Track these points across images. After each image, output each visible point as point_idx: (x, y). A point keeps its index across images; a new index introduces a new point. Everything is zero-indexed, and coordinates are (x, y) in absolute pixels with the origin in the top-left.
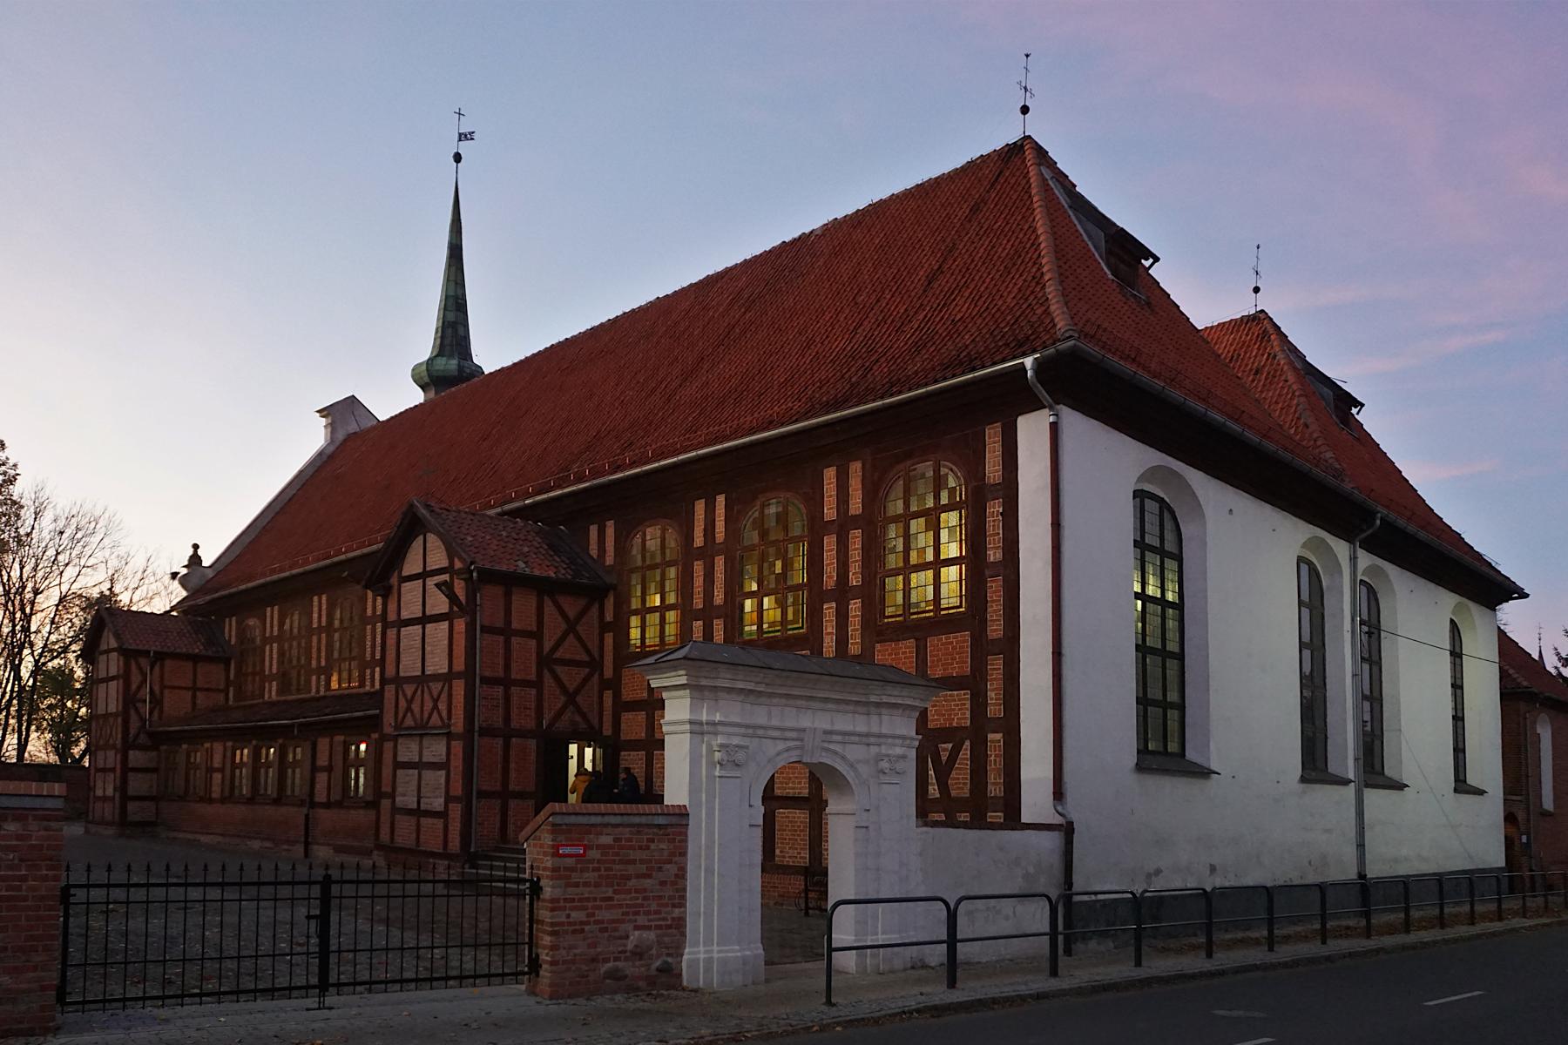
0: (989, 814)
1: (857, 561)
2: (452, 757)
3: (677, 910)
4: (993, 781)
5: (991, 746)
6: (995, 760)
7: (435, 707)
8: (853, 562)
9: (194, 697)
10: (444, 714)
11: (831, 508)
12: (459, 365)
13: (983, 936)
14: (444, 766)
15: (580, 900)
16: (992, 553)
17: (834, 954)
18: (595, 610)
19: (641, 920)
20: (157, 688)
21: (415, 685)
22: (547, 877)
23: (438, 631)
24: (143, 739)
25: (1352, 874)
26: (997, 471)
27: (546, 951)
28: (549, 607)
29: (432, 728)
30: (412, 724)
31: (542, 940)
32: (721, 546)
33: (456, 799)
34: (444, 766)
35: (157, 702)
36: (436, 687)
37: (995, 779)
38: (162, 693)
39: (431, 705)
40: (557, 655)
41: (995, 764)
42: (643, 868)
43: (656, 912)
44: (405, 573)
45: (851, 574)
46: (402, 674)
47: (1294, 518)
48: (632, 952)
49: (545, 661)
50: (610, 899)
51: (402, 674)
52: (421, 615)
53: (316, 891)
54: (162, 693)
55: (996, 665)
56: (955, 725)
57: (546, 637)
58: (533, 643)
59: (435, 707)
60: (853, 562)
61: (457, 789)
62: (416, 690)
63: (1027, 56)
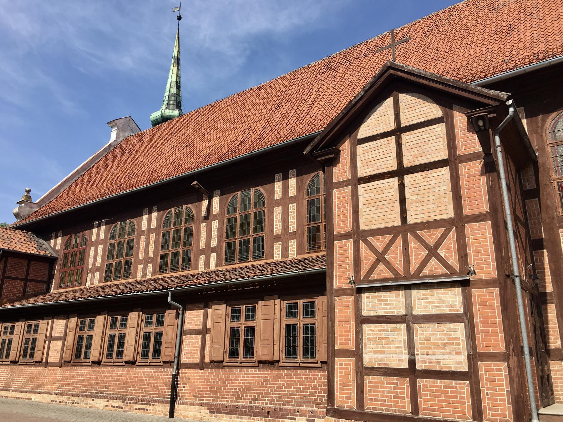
9: (25, 287)
10: (454, 261)
30: (389, 274)
46: (362, 227)
51: (362, 227)
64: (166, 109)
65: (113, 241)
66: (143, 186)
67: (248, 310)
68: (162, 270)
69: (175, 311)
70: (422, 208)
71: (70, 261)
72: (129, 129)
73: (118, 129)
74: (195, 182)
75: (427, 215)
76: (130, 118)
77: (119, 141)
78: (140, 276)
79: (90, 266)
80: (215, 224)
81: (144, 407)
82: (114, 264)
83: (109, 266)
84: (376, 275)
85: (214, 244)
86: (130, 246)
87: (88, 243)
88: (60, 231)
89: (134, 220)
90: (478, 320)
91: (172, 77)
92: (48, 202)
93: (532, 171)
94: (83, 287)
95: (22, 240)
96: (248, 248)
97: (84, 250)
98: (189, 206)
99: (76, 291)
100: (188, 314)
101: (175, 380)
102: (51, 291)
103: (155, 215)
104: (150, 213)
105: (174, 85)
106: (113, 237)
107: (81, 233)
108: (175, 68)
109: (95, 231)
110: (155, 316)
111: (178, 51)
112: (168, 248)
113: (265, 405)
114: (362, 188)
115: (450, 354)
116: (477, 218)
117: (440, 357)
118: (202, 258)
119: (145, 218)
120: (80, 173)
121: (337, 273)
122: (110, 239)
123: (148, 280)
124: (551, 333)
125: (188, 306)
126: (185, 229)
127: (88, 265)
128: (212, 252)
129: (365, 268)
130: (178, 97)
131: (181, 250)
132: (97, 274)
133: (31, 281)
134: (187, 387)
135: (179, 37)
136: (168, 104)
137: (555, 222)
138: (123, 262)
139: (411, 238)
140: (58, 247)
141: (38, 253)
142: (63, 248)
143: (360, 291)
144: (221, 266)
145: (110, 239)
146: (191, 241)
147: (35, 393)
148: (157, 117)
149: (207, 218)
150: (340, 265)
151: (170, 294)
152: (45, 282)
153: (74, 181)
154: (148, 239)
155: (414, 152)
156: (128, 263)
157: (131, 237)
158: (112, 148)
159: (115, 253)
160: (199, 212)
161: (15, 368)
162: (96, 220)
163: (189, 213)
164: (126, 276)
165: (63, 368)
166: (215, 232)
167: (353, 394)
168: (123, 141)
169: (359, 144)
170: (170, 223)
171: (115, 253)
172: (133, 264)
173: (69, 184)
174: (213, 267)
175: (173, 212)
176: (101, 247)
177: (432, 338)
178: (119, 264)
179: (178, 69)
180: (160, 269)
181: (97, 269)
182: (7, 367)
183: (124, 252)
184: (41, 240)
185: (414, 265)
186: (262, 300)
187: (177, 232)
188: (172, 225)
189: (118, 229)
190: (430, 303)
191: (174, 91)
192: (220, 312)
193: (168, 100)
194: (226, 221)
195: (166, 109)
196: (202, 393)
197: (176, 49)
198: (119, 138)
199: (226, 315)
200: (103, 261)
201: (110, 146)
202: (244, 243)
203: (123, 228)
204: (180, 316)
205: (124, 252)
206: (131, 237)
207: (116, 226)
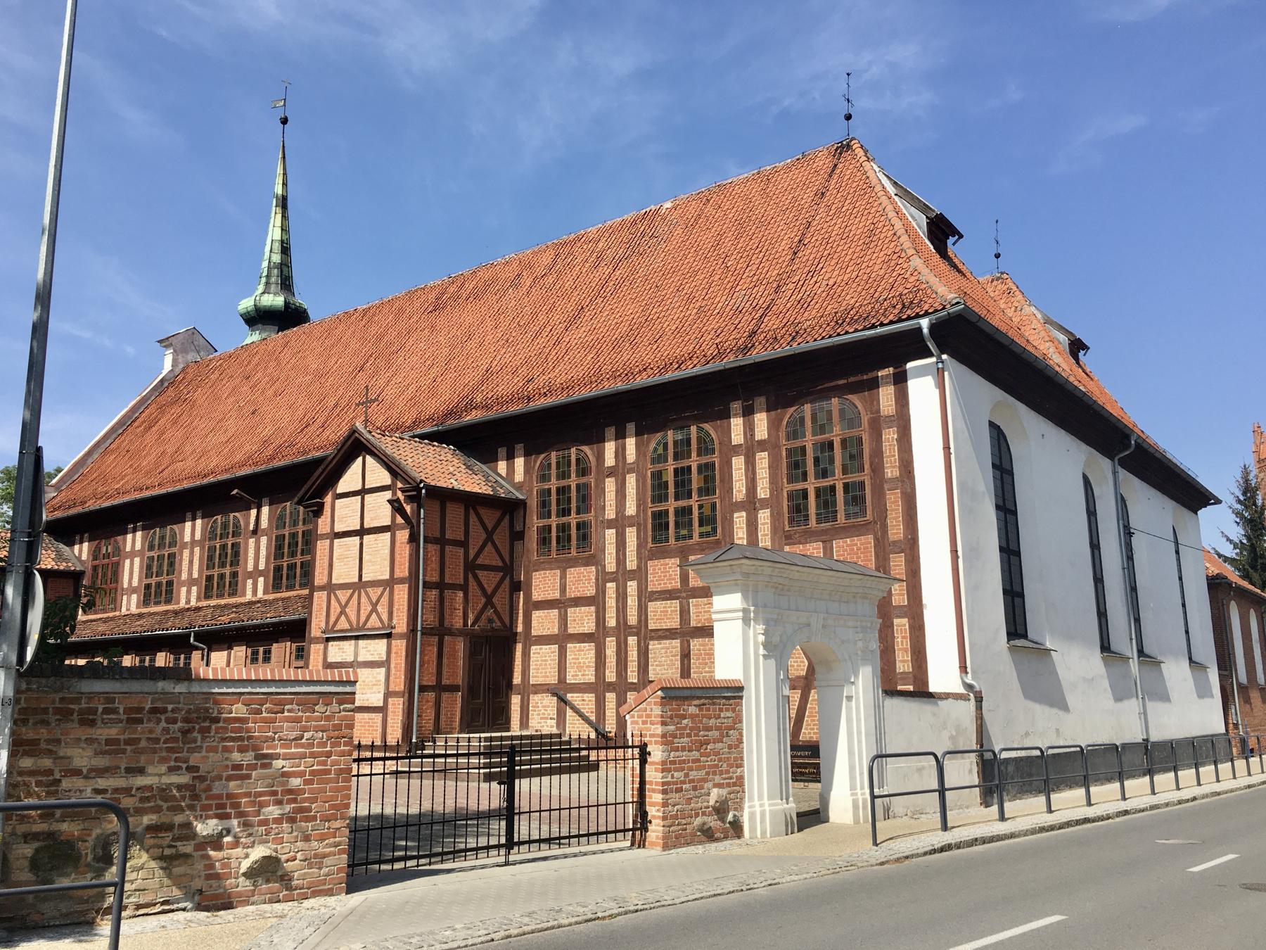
1: (764, 478)
2: (393, 655)
3: (739, 770)
4: (901, 658)
5: (897, 630)
6: (902, 642)
7: (374, 610)
8: (760, 479)
10: (385, 617)
11: (738, 435)
12: (285, 301)
13: (957, 786)
14: (386, 664)
15: (680, 762)
16: (889, 471)
17: (876, 800)
18: (506, 522)
19: (717, 779)
21: (381, 589)
22: (656, 743)
23: (378, 546)
25: (418, 813)
26: (891, 405)
27: (657, 808)
28: (473, 519)
29: (368, 629)
30: (347, 626)
31: (651, 797)
32: (633, 466)
33: (395, 694)
34: (386, 664)
36: (374, 593)
37: (903, 657)
39: (339, 610)
40: (479, 561)
41: (902, 645)
42: (715, 734)
43: (727, 772)
44: (338, 492)
45: (759, 488)
46: (334, 581)
47: (1078, 441)
48: (714, 808)
49: (471, 567)
50: (699, 761)
51: (334, 581)
52: (359, 528)
53: (636, 751)
55: (898, 564)
57: (471, 546)
58: (462, 551)
60: (760, 479)
61: (399, 684)
62: (352, 596)
64: (263, 293)
65: (152, 554)
66: (186, 485)
67: (265, 652)
68: (207, 597)
69: (200, 652)
70: (373, 567)
71: (100, 577)
72: (193, 348)
73: (175, 351)
74: (235, 492)
75: (375, 574)
76: (194, 330)
77: (177, 370)
78: (184, 601)
79: (126, 586)
80: (264, 540)
82: (154, 584)
83: (148, 587)
85: (262, 566)
86: (172, 562)
87: (122, 553)
88: (86, 532)
89: (175, 527)
90: (392, 666)
91: (275, 233)
92: (69, 482)
93: (522, 513)
94: (117, 613)
97: (118, 563)
98: (237, 514)
99: (105, 621)
100: (214, 655)
102: (79, 617)
103: (199, 522)
104: (194, 519)
105: (277, 246)
106: (151, 548)
107: (113, 539)
108: (279, 216)
109: (129, 537)
110: (182, 656)
111: (283, 184)
112: (284, 527)
115: (375, 693)
117: (369, 695)
119: (188, 525)
120: (117, 430)
122: (148, 551)
124: (515, 670)
126: (233, 544)
127: (122, 583)
128: (260, 576)
130: (285, 269)
131: (227, 571)
132: (134, 597)
135: (284, 157)
136: (267, 283)
137: (531, 565)
138: (164, 582)
139: (363, 594)
140: (84, 557)
141: (56, 567)
142: (91, 558)
143: (328, 640)
145: (148, 551)
146: (239, 560)
148: (249, 309)
149: (255, 532)
151: (192, 634)
153: (107, 444)
154: (192, 553)
156: (170, 583)
157: (174, 550)
158: (166, 384)
159: (155, 570)
160: (248, 524)
162: (130, 523)
163: (237, 525)
164: (168, 601)
166: (263, 552)
168: (183, 370)
169: (337, 499)
171: (155, 570)
172: (175, 585)
173: (100, 450)
174: (260, 594)
175: (219, 521)
176: (137, 560)
177: (367, 680)
178: (159, 585)
179: (285, 217)
180: (205, 593)
181: (134, 590)
183: (165, 568)
184: (61, 546)
186: (277, 642)
187: (224, 547)
188: (218, 538)
189: (157, 537)
190: (369, 651)
191: (277, 258)
192: (240, 654)
193: (268, 276)
194: (274, 538)
195: (263, 293)
197: (279, 180)
198: (177, 366)
199: (246, 657)
200: (140, 580)
201: (162, 381)
203: (163, 536)
204: (205, 658)
205: (165, 568)
206: (174, 550)
207: (155, 532)
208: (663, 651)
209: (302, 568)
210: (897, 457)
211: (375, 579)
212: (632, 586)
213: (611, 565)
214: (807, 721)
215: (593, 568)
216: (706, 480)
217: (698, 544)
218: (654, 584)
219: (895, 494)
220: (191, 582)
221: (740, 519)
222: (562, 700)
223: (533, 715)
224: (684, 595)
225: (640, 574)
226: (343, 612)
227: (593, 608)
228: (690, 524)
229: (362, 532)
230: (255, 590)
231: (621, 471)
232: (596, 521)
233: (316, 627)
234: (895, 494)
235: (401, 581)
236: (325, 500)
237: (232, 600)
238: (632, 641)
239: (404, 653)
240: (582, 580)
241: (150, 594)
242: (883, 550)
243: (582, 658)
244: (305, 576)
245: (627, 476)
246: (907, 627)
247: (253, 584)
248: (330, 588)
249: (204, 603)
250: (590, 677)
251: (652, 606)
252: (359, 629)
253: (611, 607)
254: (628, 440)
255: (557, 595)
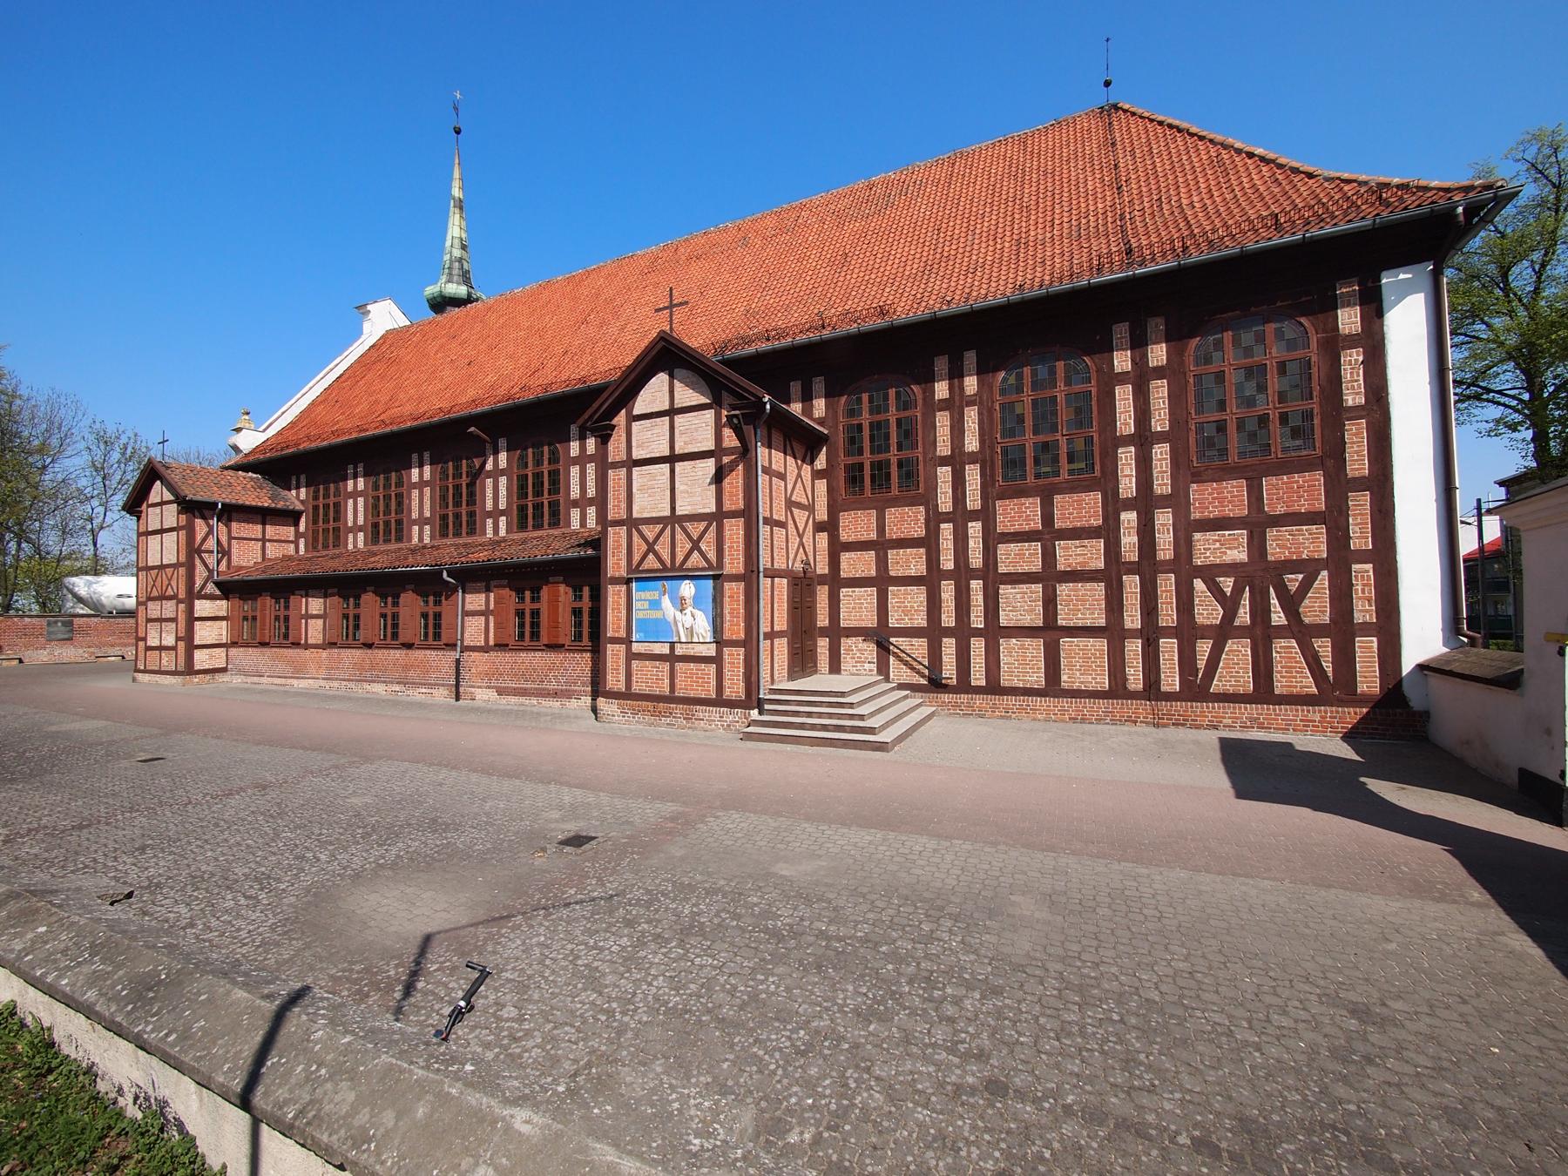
0: (1357, 639)
4: (1360, 608)
9: (264, 549)
10: (712, 556)
20: (224, 539)
24: (211, 588)
30: (658, 565)
35: (224, 552)
38: (229, 544)
44: (636, 411)
46: (635, 515)
54: (229, 544)
55: (1360, 506)
56: (1304, 556)
59: (154, 582)
61: (182, 634)
63: (1108, 40)
68: (444, 535)
79: (350, 524)
81: (429, 691)
84: (645, 566)
85: (502, 505)
95: (249, 486)
96: (543, 513)
101: (458, 662)
113: (553, 686)
114: (636, 470)
116: (734, 514)
118: (489, 522)
121: (610, 561)
123: (424, 547)
125: (468, 585)
129: (636, 558)
133: (269, 541)
134: (473, 670)
139: (678, 529)
141: (273, 505)
144: (512, 532)
147: (298, 678)
150: (613, 553)
152: (291, 542)
155: (685, 438)
159: (382, 509)
161: (267, 651)
164: (399, 539)
165: (328, 651)
166: (503, 491)
167: (622, 678)
170: (448, 475)
174: (502, 532)
182: (255, 649)
185: (680, 557)
196: (488, 675)
202: (538, 507)
208: (1018, 596)
209: (550, 507)
210: (1362, 382)
211: (694, 512)
212: (975, 528)
213: (945, 502)
214: (1222, 673)
215: (922, 508)
216: (1078, 411)
217: (1067, 481)
218: (1004, 523)
219: (1358, 424)
220: (422, 522)
221: (944, 473)
222: (884, 648)
223: (845, 658)
224: (1047, 537)
225: (986, 515)
226: (170, 580)
227: (922, 550)
228: (1056, 460)
229: (672, 459)
230: (422, 535)
231: (957, 404)
232: (924, 458)
233: (615, 564)
234: (1358, 424)
235: (734, 514)
236: (614, 422)
237: (469, 540)
238: (976, 585)
239: (742, 598)
240: (907, 521)
241: (376, 532)
242: (1339, 487)
243: (909, 602)
244: (554, 511)
245: (966, 409)
246: (1371, 573)
247: (493, 523)
248: (632, 523)
249: (516, 536)
250: (921, 620)
251: (1002, 549)
252: (673, 568)
253: (947, 549)
254: (425, 468)
255: (873, 536)
